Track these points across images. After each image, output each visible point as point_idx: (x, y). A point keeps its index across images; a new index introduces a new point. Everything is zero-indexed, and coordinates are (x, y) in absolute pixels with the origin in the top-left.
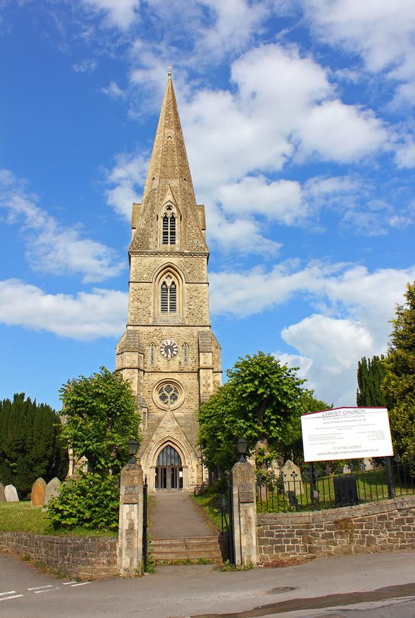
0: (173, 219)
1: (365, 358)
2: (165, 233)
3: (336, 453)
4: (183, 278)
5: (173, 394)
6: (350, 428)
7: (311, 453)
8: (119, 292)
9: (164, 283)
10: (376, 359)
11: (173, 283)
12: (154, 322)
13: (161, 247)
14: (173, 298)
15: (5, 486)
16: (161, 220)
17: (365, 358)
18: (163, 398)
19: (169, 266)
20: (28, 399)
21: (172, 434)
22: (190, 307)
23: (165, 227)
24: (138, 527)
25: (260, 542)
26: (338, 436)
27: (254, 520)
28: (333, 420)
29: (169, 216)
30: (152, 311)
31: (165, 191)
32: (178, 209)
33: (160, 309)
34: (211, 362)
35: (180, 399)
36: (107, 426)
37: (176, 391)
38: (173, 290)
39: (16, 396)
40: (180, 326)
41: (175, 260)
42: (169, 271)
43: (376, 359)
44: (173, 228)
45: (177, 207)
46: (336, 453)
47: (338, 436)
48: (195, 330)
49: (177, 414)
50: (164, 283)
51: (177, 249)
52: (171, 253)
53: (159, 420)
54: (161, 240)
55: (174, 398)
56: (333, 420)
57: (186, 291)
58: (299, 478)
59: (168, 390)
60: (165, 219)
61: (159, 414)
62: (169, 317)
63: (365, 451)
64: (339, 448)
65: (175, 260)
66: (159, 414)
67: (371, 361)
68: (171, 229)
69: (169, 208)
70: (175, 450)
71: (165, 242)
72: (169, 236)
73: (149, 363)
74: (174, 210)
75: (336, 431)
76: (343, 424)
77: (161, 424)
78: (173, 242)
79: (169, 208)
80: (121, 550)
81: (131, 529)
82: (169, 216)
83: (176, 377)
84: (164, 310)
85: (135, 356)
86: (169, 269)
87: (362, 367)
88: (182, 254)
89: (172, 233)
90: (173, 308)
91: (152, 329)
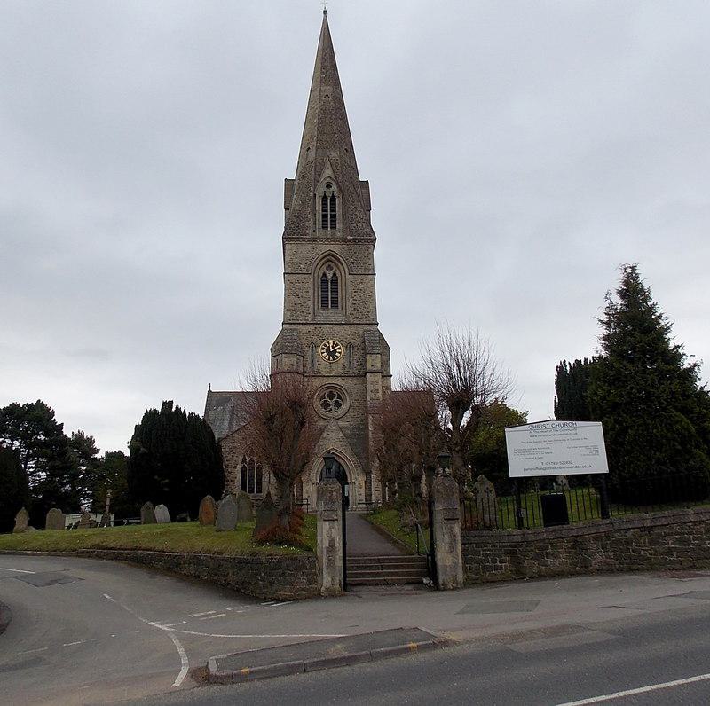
0: (333, 199)
1: (565, 362)
2: (325, 216)
3: (545, 469)
4: (347, 269)
5: (337, 401)
6: (560, 442)
7: (516, 469)
8: (674, 339)
9: (324, 274)
10: (578, 362)
11: (335, 274)
12: (314, 319)
13: (320, 233)
14: (335, 292)
15: (155, 506)
16: (319, 201)
17: (565, 362)
18: (326, 405)
19: (329, 255)
20: (177, 408)
21: (337, 446)
22: (355, 302)
23: (325, 209)
24: (339, 544)
25: (465, 562)
26: (546, 451)
27: (459, 538)
28: (541, 434)
29: (329, 195)
30: (312, 307)
31: (323, 165)
32: (339, 187)
33: (320, 305)
34: (379, 367)
35: (345, 407)
36: (32, 456)
37: (339, 397)
38: (335, 282)
39: (164, 403)
40: (343, 324)
41: (336, 248)
42: (329, 260)
43: (578, 362)
44: (333, 209)
45: (337, 183)
46: (545, 469)
47: (546, 451)
48: (360, 329)
49: (341, 423)
50: (324, 274)
51: (339, 235)
52: (332, 239)
53: (322, 430)
54: (319, 224)
55: (338, 405)
56: (541, 434)
57: (349, 284)
58: (493, 495)
59: (331, 396)
60: (325, 199)
61: (321, 423)
62: (333, 315)
63: (576, 467)
64: (547, 464)
65: (336, 248)
66: (321, 423)
67: (572, 366)
68: (331, 211)
69: (329, 186)
70: (340, 464)
71: (325, 226)
72: (329, 220)
73: (309, 366)
74: (334, 188)
75: (544, 445)
76: (552, 438)
77: (325, 435)
78: (334, 226)
79: (329, 186)
80: (321, 569)
81: (332, 546)
82: (329, 195)
83: (340, 381)
84: (325, 306)
85: (294, 359)
86: (330, 258)
87: (561, 370)
88: (344, 240)
89: (334, 217)
90: (335, 304)
91: (313, 327)
